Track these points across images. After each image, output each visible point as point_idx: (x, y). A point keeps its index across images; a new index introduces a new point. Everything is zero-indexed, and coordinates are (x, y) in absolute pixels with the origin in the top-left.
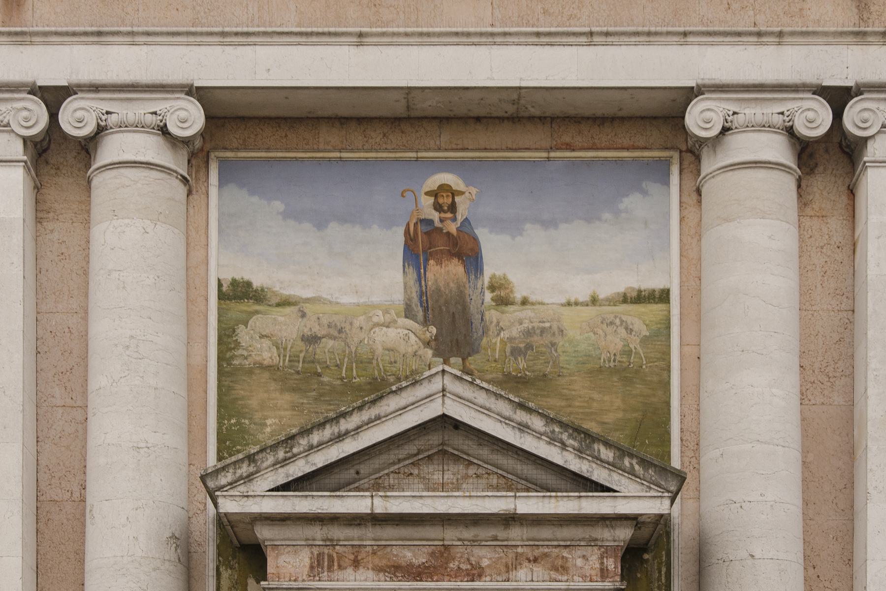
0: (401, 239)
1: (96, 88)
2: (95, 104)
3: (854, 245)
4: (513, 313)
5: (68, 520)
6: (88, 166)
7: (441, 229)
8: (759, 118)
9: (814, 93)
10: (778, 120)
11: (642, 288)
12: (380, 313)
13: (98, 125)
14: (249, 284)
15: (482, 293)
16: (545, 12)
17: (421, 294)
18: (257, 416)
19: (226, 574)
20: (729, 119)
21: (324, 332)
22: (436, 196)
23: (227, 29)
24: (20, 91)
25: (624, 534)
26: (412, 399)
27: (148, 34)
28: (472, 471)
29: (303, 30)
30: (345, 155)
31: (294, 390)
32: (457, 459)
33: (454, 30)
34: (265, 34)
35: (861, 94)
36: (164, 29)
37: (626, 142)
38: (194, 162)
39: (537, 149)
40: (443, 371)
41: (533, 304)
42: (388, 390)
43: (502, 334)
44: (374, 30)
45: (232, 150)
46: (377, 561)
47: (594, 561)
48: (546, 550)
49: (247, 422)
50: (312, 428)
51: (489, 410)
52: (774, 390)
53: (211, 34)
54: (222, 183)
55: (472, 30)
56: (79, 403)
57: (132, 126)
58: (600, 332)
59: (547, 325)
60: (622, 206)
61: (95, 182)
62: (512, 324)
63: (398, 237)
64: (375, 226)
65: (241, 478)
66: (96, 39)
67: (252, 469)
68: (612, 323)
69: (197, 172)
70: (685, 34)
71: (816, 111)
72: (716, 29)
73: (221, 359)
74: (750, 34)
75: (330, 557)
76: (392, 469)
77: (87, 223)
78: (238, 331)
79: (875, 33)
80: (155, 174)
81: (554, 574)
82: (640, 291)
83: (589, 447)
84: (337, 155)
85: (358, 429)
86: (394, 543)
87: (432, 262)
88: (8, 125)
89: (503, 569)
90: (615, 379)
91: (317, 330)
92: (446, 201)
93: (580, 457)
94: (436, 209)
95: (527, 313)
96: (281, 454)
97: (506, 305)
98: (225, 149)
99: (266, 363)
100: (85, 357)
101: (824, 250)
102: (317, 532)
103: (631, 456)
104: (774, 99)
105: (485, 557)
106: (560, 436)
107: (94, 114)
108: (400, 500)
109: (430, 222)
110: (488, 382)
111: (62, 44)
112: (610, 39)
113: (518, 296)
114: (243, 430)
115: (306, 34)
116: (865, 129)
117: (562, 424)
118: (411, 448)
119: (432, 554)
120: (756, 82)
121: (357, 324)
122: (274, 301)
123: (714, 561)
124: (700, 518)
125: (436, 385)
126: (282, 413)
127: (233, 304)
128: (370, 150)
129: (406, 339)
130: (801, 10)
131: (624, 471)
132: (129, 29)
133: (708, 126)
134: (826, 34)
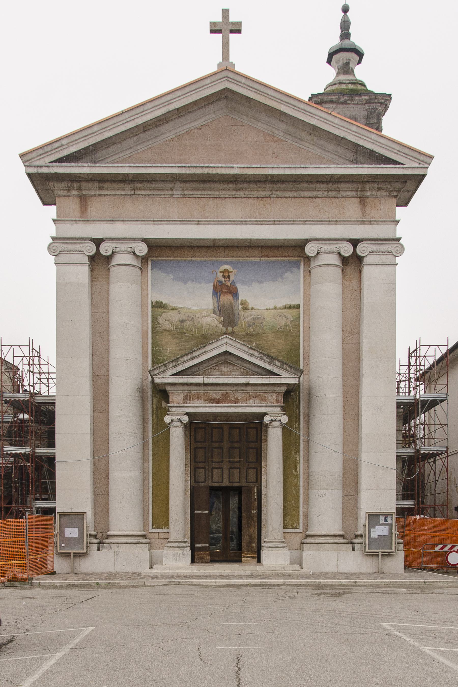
0: (212, 287)
1: (112, 239)
2: (111, 245)
3: (361, 290)
4: (249, 312)
5: (103, 382)
6: (108, 264)
7: (225, 284)
8: (329, 250)
9: (347, 241)
10: (335, 250)
11: (291, 304)
12: (205, 312)
13: (113, 251)
14: (162, 303)
15: (238, 306)
16: (259, 213)
17: (219, 306)
18: (165, 347)
19: (155, 400)
20: (319, 250)
21: (186, 319)
22: (223, 273)
23: (155, 219)
24: (87, 240)
25: (284, 389)
26: (216, 346)
27: (129, 221)
28: (235, 368)
29: (180, 220)
30: (193, 259)
31: (176, 338)
32: (230, 364)
33: (229, 220)
34: (167, 221)
35: (363, 241)
36: (134, 219)
37: (286, 254)
38: (143, 261)
40: (226, 337)
41: (255, 309)
42: (208, 343)
43: (245, 319)
44: (203, 220)
45: (155, 257)
46: (205, 397)
47: (274, 397)
48: (259, 394)
49: (161, 349)
50: (184, 355)
51: (241, 349)
53: (150, 221)
54: (152, 269)
55: (235, 220)
56: (106, 343)
57: (124, 252)
58: (277, 319)
59: (260, 316)
60: (285, 276)
61: (111, 270)
62: (248, 316)
63: (210, 288)
64: (203, 283)
65: (162, 371)
66: (111, 222)
67: (165, 369)
68: (281, 316)
69: (144, 264)
70: (305, 221)
71: (348, 247)
72: (315, 220)
73: (152, 328)
74: (326, 221)
75: (190, 396)
76: (209, 367)
77: (108, 283)
78: (158, 318)
79: (367, 221)
80: (131, 268)
81: (262, 402)
82: (290, 305)
83: (273, 362)
84: (190, 259)
85: (199, 356)
86: (210, 391)
87: (222, 295)
88: (83, 251)
89: (245, 400)
91: (184, 318)
92: (226, 274)
93: (270, 365)
94: (223, 277)
95: (253, 312)
96: (174, 364)
97: (246, 310)
98: (153, 257)
99: (167, 329)
100: (108, 327)
101: (351, 292)
102: (186, 388)
103: (286, 364)
105: (239, 396)
106: (263, 358)
107: (111, 248)
108: (212, 379)
109: (221, 282)
110: (241, 340)
111: (100, 224)
112: (280, 223)
113: (250, 307)
114: (160, 352)
115: (181, 221)
116: (363, 253)
117: (264, 354)
118: (216, 361)
119: (222, 395)
121: (197, 316)
122: (171, 308)
123: (313, 396)
124: (309, 382)
125: (224, 341)
126: (173, 346)
127: (156, 309)
128: (202, 257)
129: (213, 321)
130: (343, 212)
131: (284, 369)
132: (122, 219)
133: (312, 252)
134: (351, 221)
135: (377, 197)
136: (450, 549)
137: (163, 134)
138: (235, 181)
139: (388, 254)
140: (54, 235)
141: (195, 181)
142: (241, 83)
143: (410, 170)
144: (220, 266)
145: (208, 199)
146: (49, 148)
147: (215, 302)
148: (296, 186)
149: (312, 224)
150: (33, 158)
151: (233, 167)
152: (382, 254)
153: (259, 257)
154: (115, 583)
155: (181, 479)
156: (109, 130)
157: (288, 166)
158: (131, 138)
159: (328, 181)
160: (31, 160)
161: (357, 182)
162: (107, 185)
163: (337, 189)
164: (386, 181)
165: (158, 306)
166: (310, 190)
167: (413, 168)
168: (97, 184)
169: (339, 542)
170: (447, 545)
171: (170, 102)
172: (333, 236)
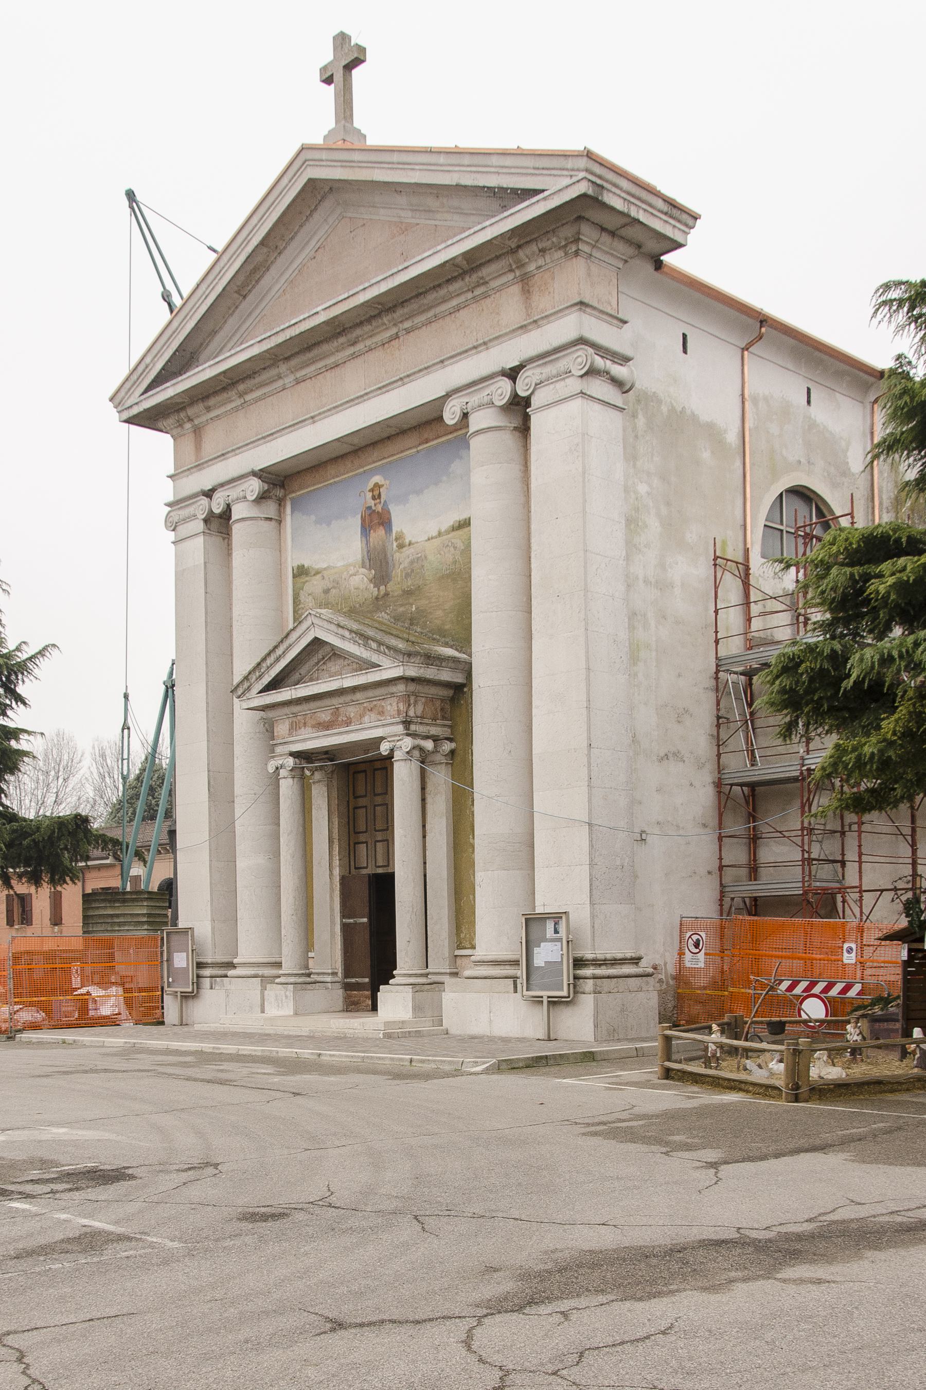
1: (222, 485)
4: (407, 551)
12: (352, 568)
26: (301, 632)
28: (346, 662)
39: (411, 448)
52: (490, 577)
60: (451, 470)
66: (223, 458)
67: (249, 684)
70: (442, 362)
87: (372, 531)
90: (449, 581)
98: (293, 492)
104: (483, 387)
112: (411, 378)
120: (471, 381)
135: (547, 267)
136: (807, 990)
137: (270, 289)
138: (344, 331)
139: (567, 377)
140: (171, 498)
141: (298, 353)
142: (322, 160)
143: (555, 197)
144: (369, 480)
145: (325, 373)
146: (135, 377)
147: (364, 546)
148: (422, 302)
149: (454, 363)
150: (124, 398)
151: (317, 313)
152: (558, 381)
153: (414, 447)
154: (83, 1041)
155: (291, 867)
156: (190, 318)
157: (382, 277)
158: (232, 315)
159: (462, 274)
160: (121, 401)
161: (503, 254)
162: (212, 402)
163: (481, 281)
164: (548, 232)
165: (301, 572)
166: (444, 301)
167: (560, 190)
168: (201, 406)
169: (498, 976)
170: (799, 982)
171: (247, 240)
172: (475, 376)
